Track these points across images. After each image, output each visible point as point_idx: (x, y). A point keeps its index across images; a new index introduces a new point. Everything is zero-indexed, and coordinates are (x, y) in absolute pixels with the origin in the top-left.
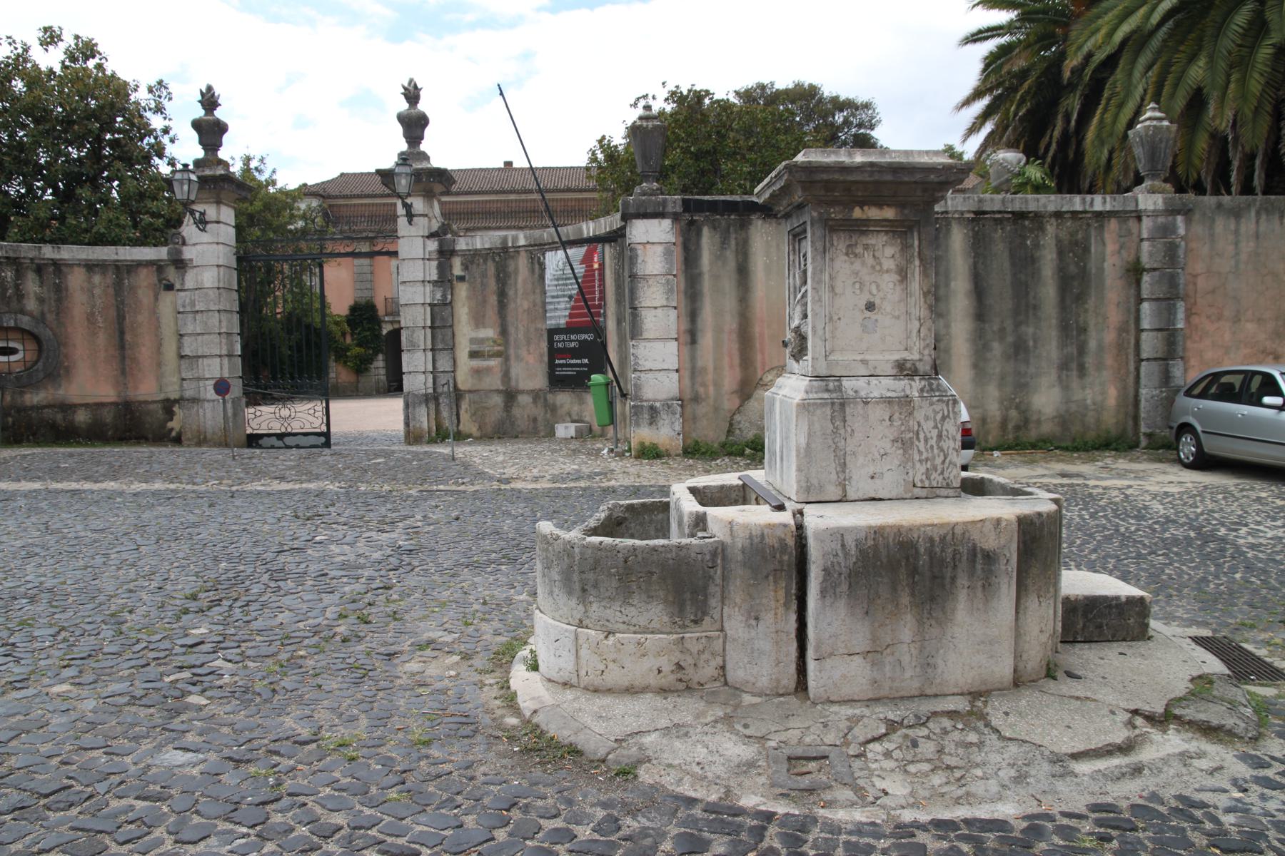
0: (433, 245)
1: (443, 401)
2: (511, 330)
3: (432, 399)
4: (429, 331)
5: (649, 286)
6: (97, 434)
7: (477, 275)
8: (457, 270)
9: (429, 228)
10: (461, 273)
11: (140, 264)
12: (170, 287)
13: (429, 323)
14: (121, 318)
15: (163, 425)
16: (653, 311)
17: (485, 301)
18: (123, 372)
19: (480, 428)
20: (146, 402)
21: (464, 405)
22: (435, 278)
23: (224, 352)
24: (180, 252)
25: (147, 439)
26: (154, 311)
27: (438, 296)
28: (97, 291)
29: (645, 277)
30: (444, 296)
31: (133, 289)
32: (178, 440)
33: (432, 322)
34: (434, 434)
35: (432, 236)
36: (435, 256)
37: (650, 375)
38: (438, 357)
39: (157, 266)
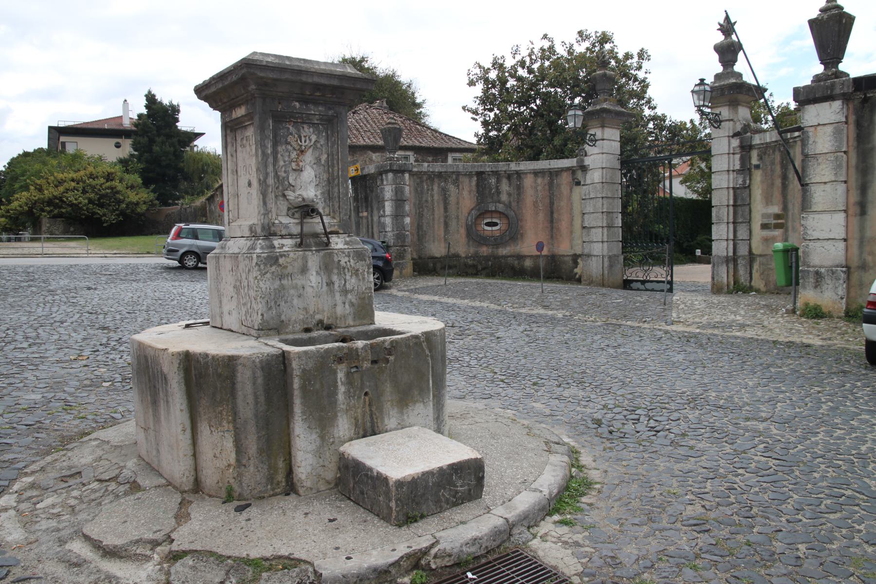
0: (736, 142)
1: (741, 262)
2: (790, 206)
3: (733, 260)
4: (731, 209)
5: (819, 164)
6: (533, 274)
7: (768, 163)
8: (755, 161)
9: (734, 129)
10: (758, 163)
11: (563, 170)
12: (578, 184)
13: (731, 202)
14: (552, 204)
15: (572, 271)
16: (822, 186)
17: (773, 184)
18: (552, 237)
19: (766, 285)
20: (563, 256)
21: (756, 266)
22: (738, 167)
23: (605, 225)
24: (583, 161)
25: (562, 279)
26: (570, 198)
27: (740, 181)
28: (539, 188)
29: (815, 156)
30: (744, 181)
31: (559, 185)
32: (579, 281)
33: (735, 200)
34: (731, 287)
35: (736, 135)
36: (738, 150)
37: (818, 244)
38: (738, 228)
39: (572, 170)
